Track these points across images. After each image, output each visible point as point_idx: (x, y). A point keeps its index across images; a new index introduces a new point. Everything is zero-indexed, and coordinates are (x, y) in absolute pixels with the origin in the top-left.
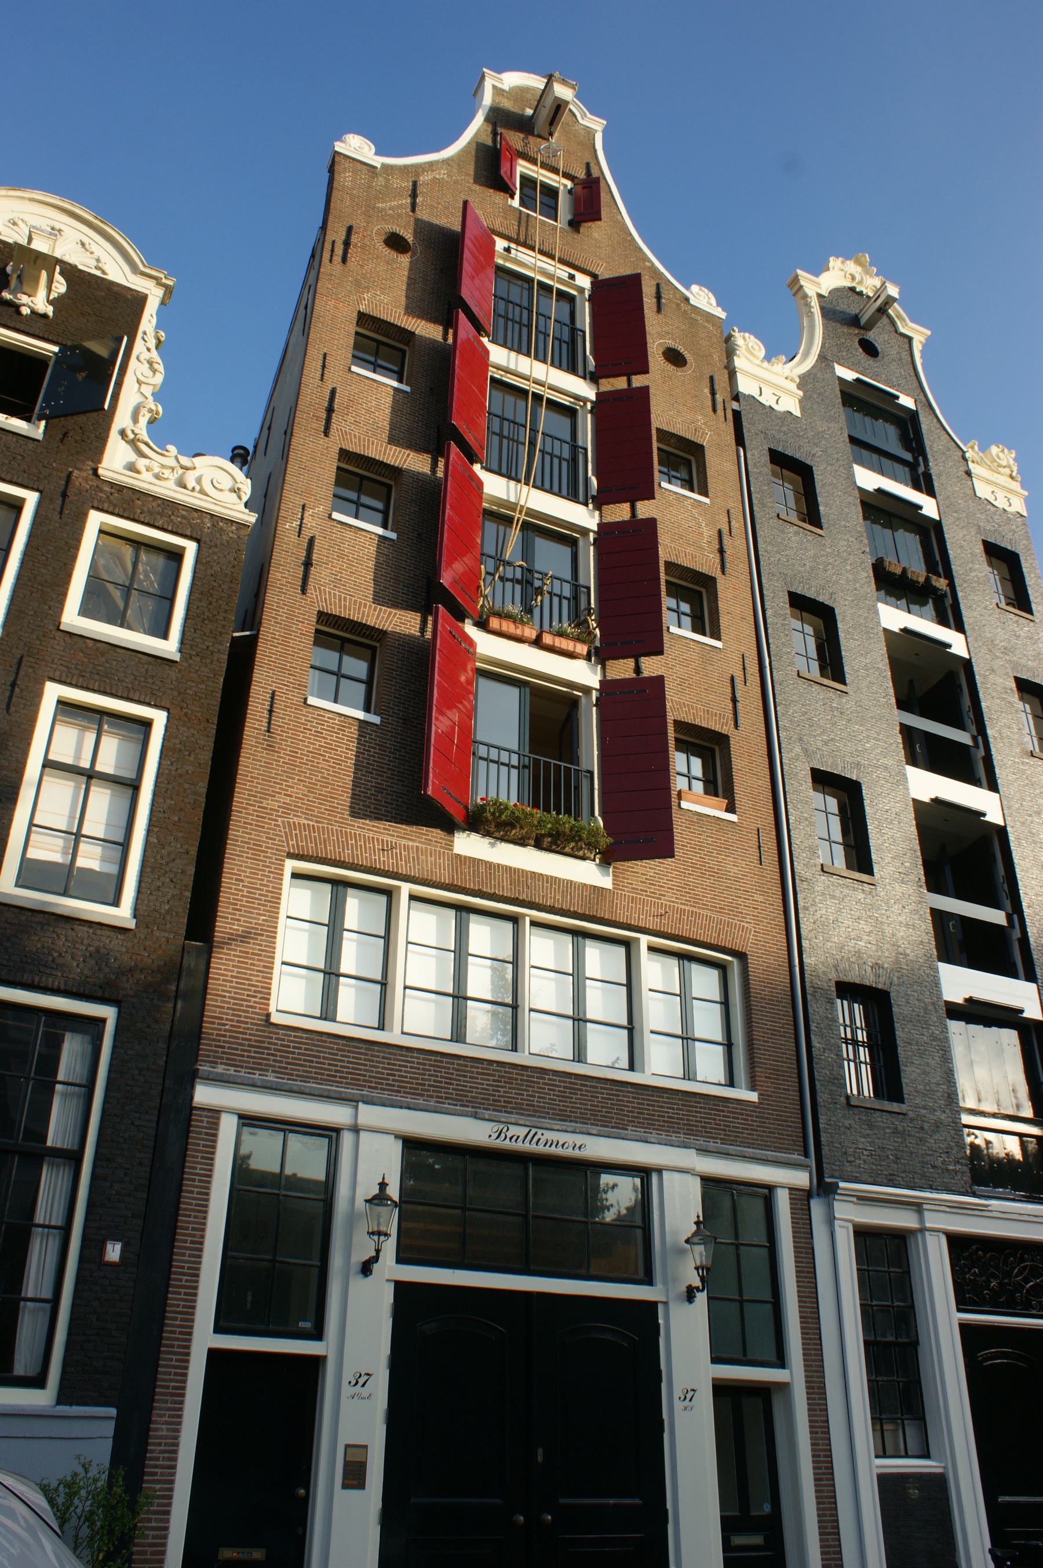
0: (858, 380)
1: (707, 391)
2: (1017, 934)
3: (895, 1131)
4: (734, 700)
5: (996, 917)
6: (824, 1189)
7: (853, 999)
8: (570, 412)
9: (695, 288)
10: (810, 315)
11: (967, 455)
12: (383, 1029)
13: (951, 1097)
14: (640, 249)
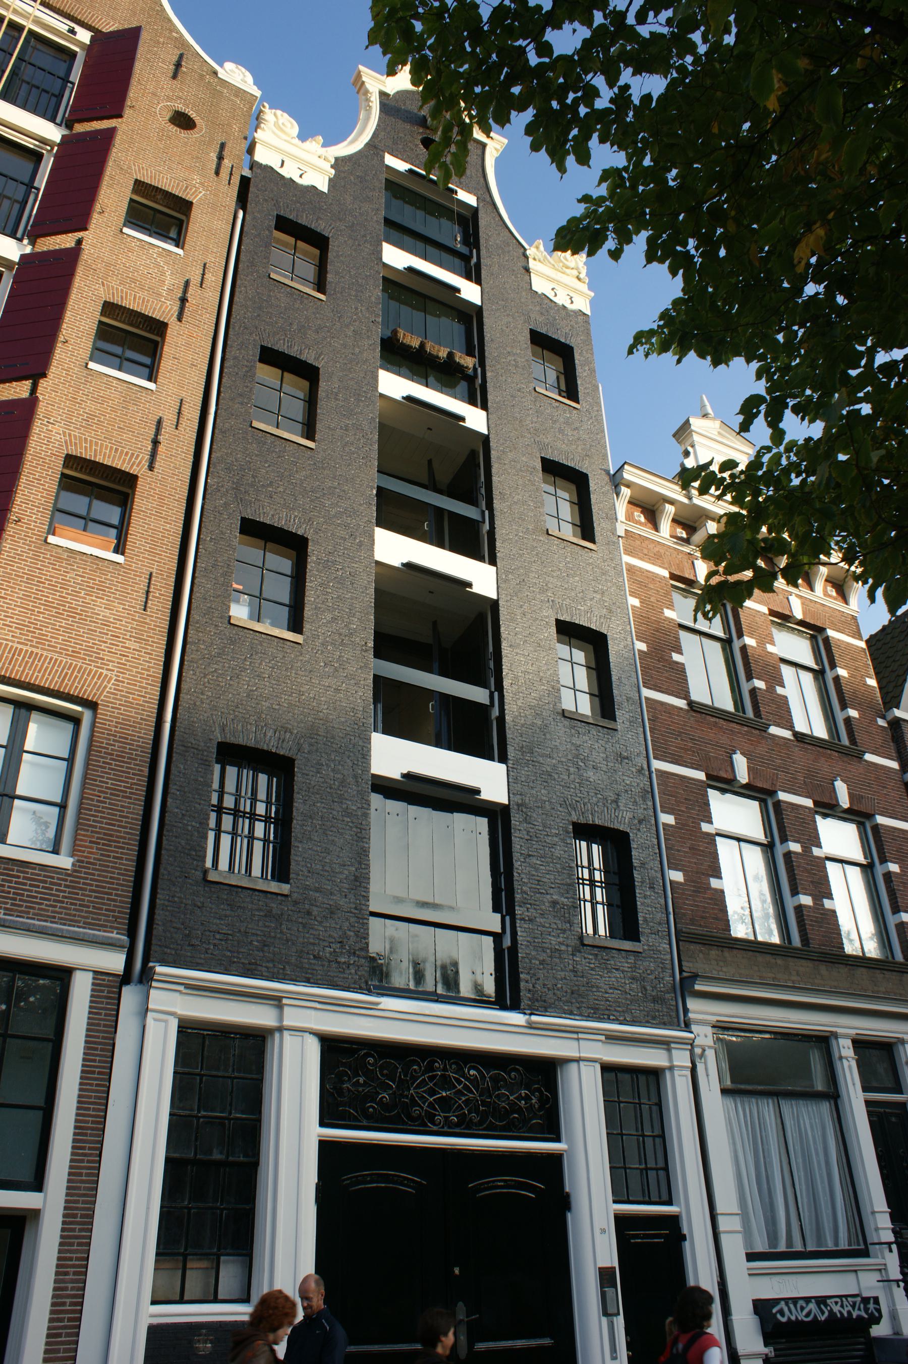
0: (410, 171)
1: (214, 156)
2: (495, 712)
3: (269, 914)
4: (156, 442)
5: (477, 694)
6: (137, 975)
7: (590, 841)
8: (36, 157)
9: (229, 66)
10: (369, 109)
11: (528, 252)
12: (57, 853)
13: (360, 882)
14: (170, 20)
